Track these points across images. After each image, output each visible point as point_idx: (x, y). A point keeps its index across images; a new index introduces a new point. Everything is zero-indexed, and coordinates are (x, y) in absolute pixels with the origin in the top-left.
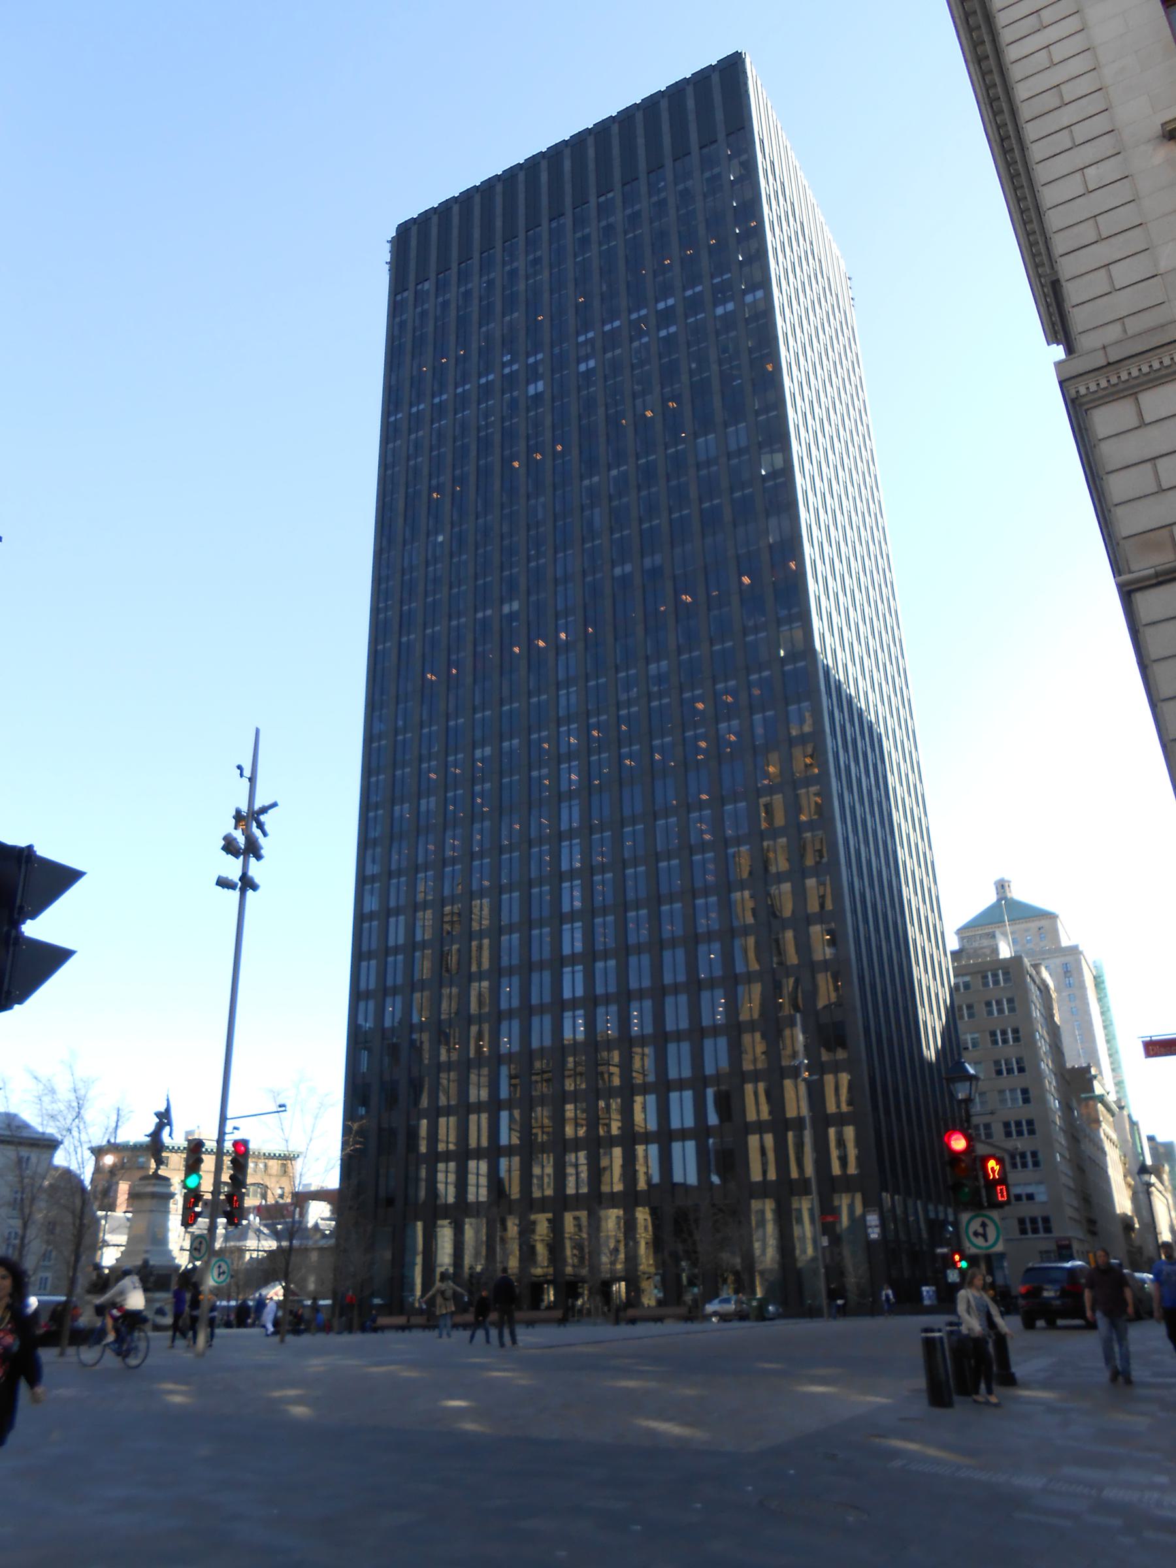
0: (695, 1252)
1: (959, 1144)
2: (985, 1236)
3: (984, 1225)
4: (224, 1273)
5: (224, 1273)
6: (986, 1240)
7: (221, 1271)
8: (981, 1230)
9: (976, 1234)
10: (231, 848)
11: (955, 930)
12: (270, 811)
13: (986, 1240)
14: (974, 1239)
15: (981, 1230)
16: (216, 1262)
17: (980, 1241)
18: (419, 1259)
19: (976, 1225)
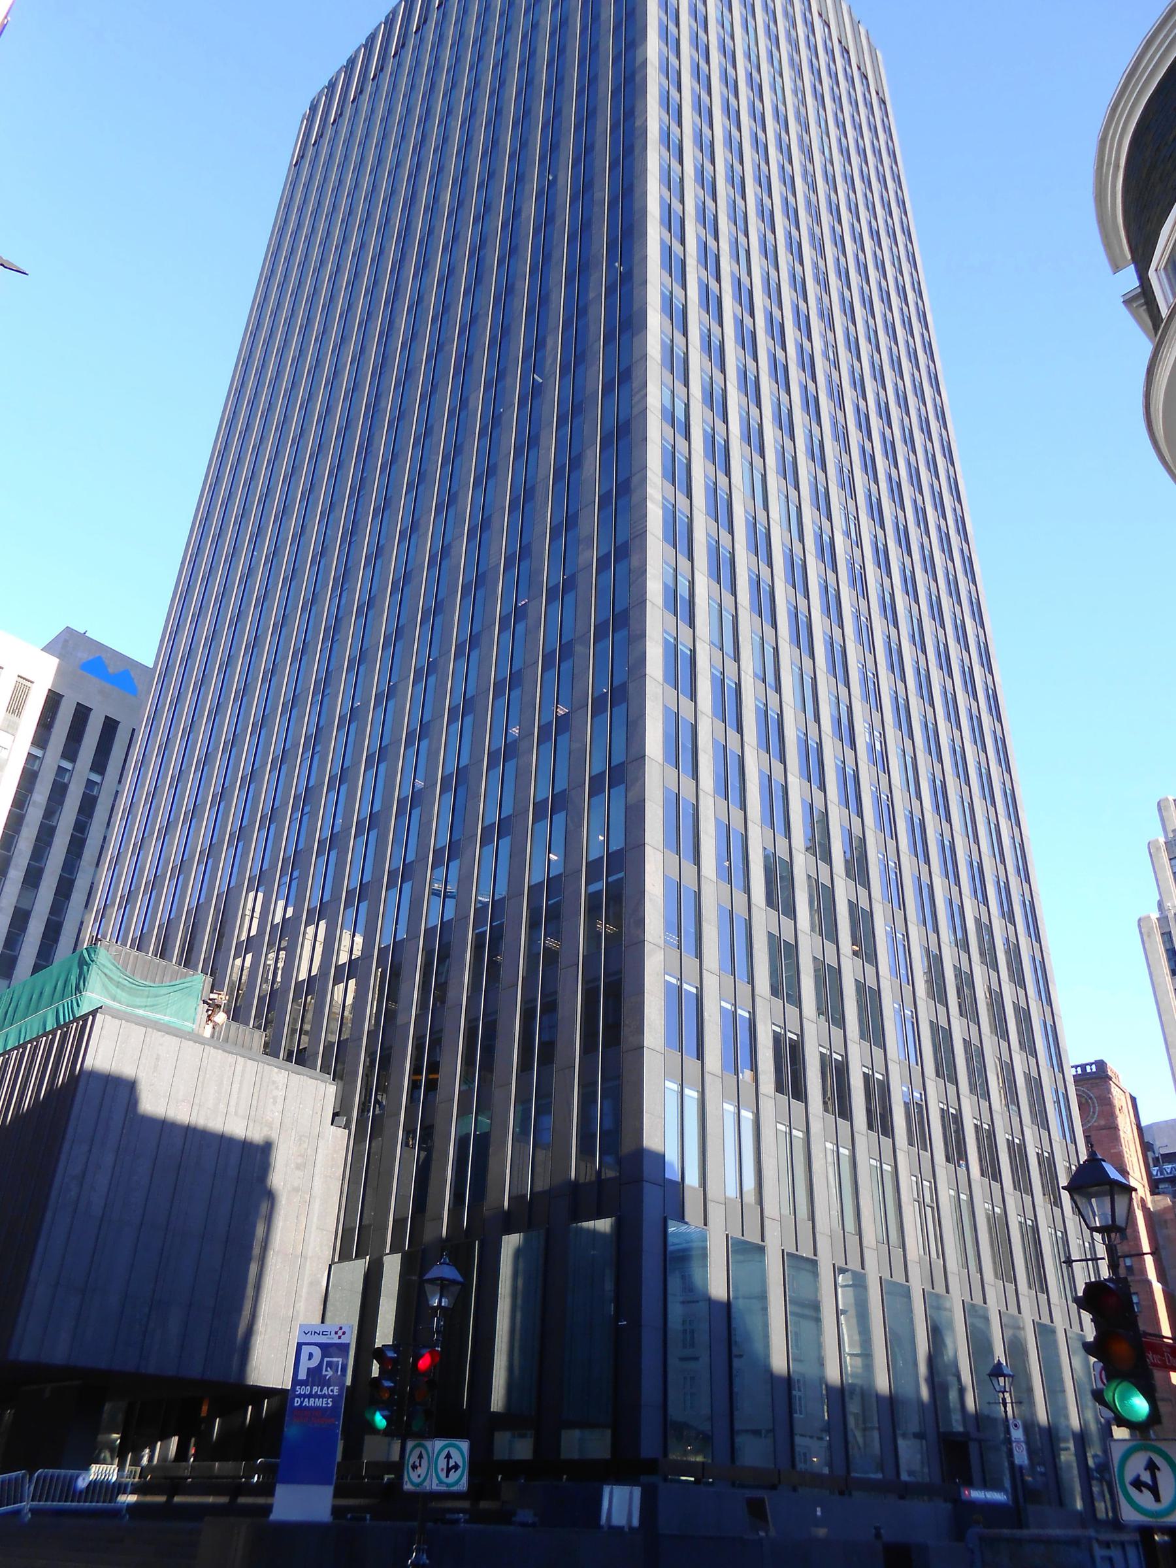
0: (148, 997)
1: (1127, 1315)
2: (1155, 1490)
3: (1152, 1467)
4: (456, 1467)
5: (456, 1467)
6: (1157, 1499)
7: (452, 1463)
8: (1146, 1477)
9: (1138, 1484)
10: (808, 1266)
11: (1113, 1066)
12: (670, 322)
13: (1157, 1499)
14: (1132, 1491)
15: (1146, 1477)
16: (415, 1447)
17: (1145, 1499)
18: (219, 1480)
19: (456, 1458)
